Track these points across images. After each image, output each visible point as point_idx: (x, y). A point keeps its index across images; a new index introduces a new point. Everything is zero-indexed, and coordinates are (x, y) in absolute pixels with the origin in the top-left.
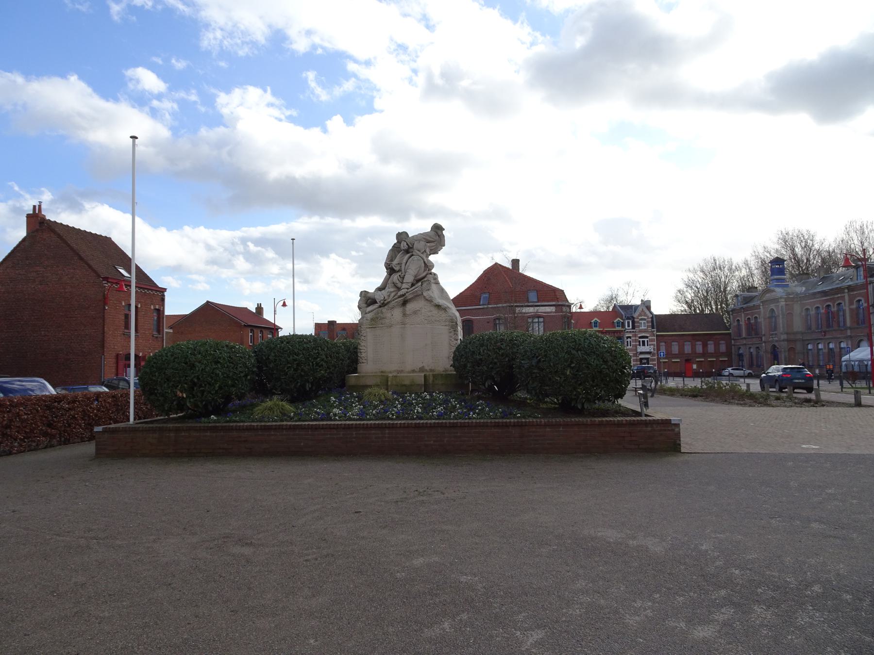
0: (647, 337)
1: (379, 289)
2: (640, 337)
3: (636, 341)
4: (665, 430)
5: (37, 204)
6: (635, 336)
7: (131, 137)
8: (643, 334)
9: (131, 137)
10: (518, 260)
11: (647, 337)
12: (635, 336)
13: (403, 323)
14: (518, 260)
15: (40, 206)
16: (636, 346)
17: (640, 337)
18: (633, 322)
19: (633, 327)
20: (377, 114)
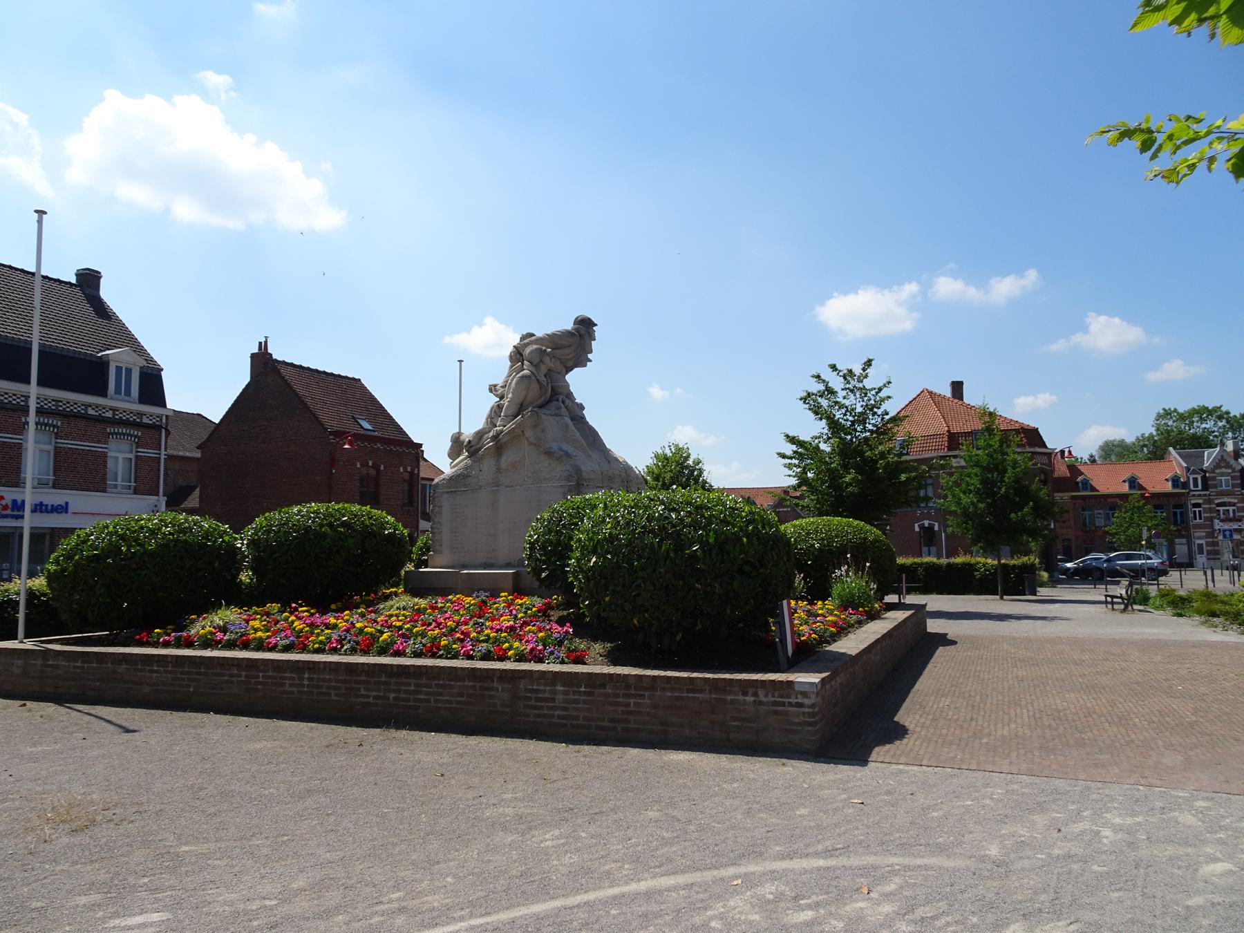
0: (1234, 505)
1: (1114, 452)
2: (1219, 505)
3: (1211, 510)
4: (783, 704)
5: (263, 340)
6: (1210, 501)
7: (36, 211)
8: (1226, 499)
9: (36, 211)
10: (962, 383)
11: (1234, 505)
12: (1210, 501)
13: (497, 484)
14: (962, 383)
15: (266, 342)
16: (1211, 519)
17: (1219, 505)
18: (1204, 479)
19: (1205, 487)
20: (195, 100)
